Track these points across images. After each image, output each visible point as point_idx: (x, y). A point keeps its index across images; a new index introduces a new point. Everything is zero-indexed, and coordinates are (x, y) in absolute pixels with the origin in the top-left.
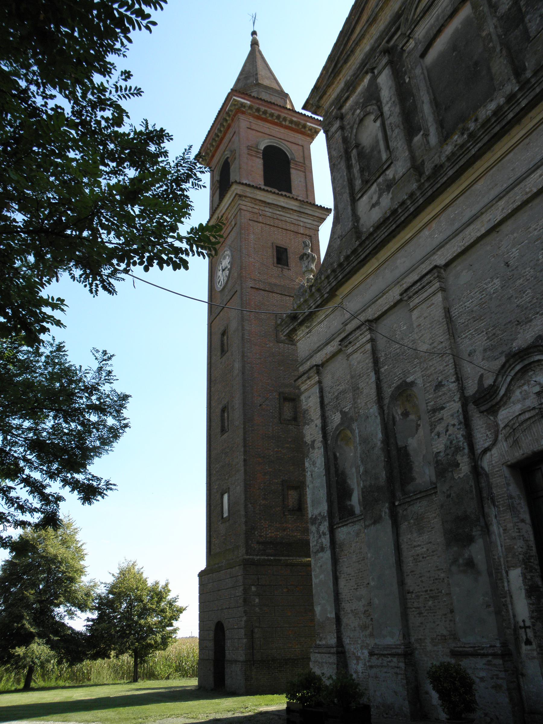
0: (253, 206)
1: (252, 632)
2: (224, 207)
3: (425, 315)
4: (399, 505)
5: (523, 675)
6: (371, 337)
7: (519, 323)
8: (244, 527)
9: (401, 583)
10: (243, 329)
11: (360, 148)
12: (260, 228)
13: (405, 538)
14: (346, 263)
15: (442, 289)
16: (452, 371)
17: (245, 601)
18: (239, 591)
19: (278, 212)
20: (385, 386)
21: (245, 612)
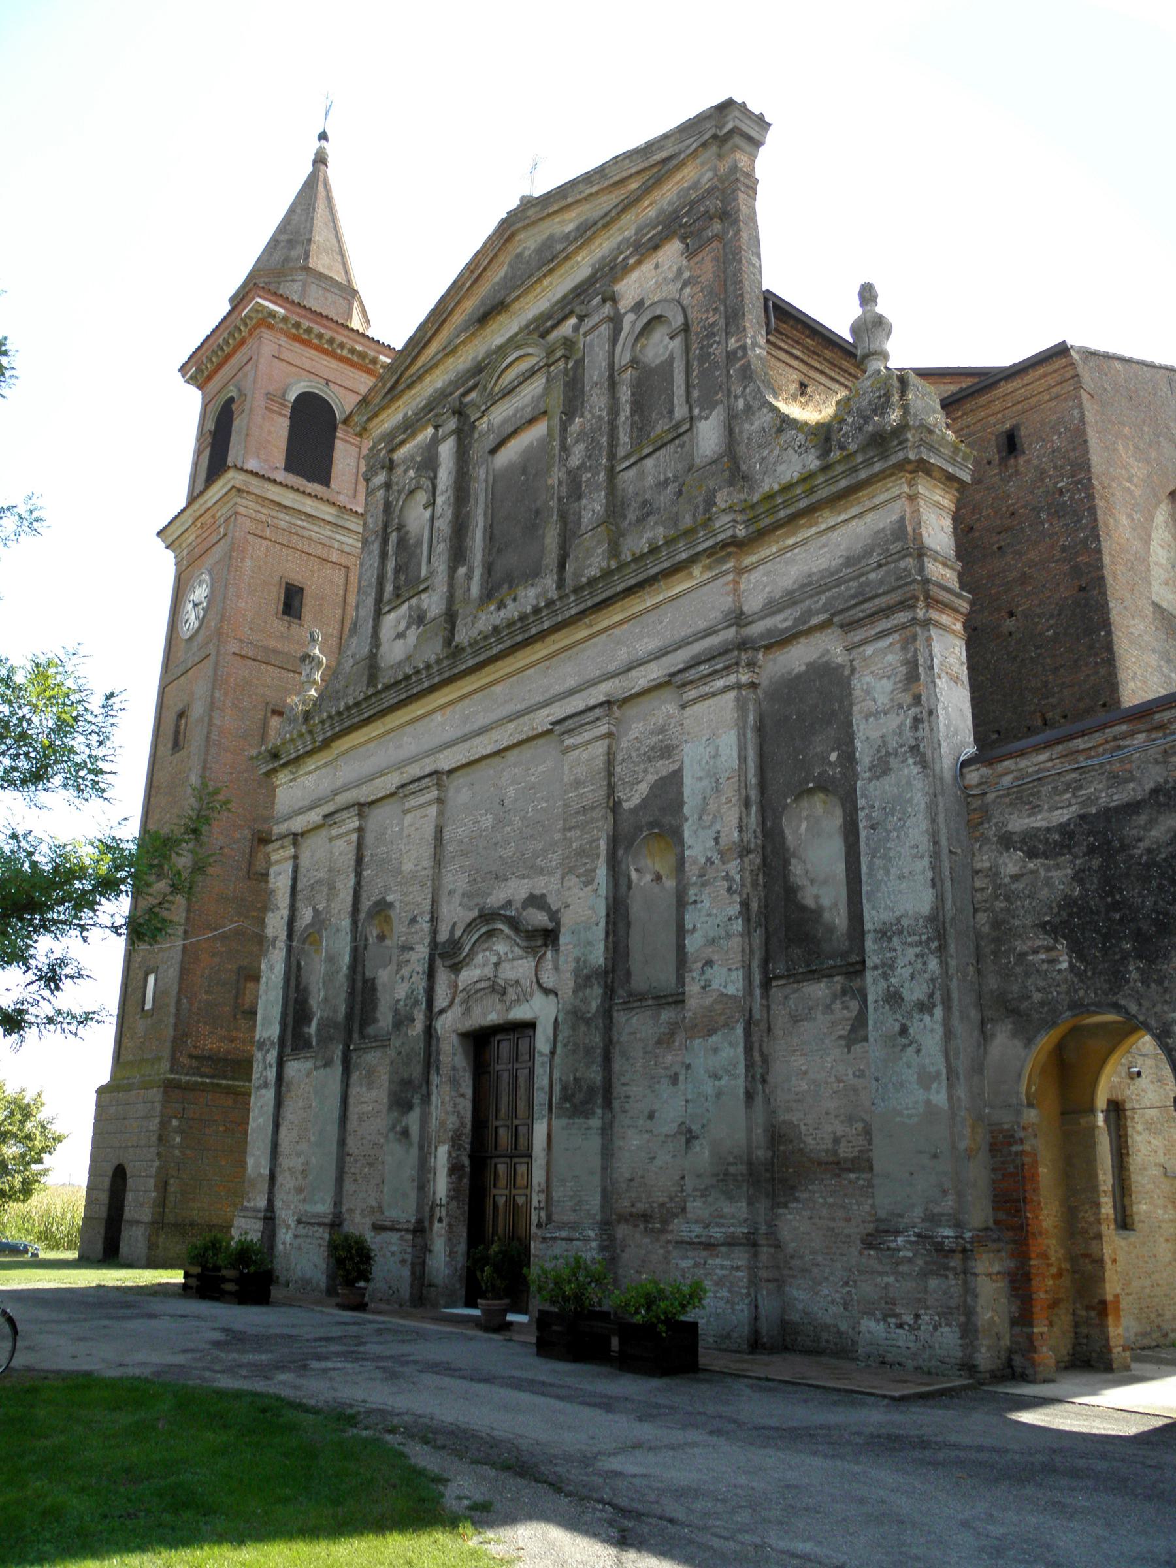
0: (259, 508)
1: (166, 1183)
2: (211, 497)
3: (417, 826)
4: (355, 1050)
5: (430, 1251)
6: (360, 824)
7: (497, 877)
8: (171, 1032)
9: (342, 1142)
10: (210, 724)
11: (403, 531)
12: (263, 549)
13: (353, 1091)
14: (346, 714)
15: (440, 801)
16: (428, 908)
17: (160, 1139)
18: (154, 1125)
19: (299, 523)
20: (364, 896)
21: (159, 1154)
